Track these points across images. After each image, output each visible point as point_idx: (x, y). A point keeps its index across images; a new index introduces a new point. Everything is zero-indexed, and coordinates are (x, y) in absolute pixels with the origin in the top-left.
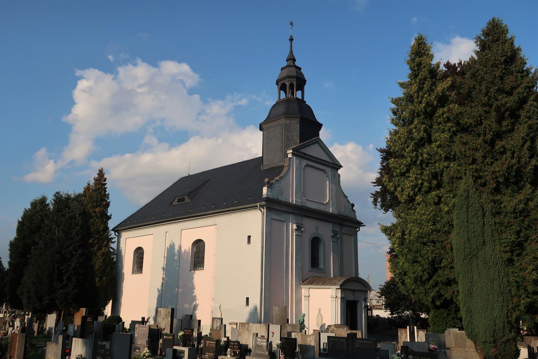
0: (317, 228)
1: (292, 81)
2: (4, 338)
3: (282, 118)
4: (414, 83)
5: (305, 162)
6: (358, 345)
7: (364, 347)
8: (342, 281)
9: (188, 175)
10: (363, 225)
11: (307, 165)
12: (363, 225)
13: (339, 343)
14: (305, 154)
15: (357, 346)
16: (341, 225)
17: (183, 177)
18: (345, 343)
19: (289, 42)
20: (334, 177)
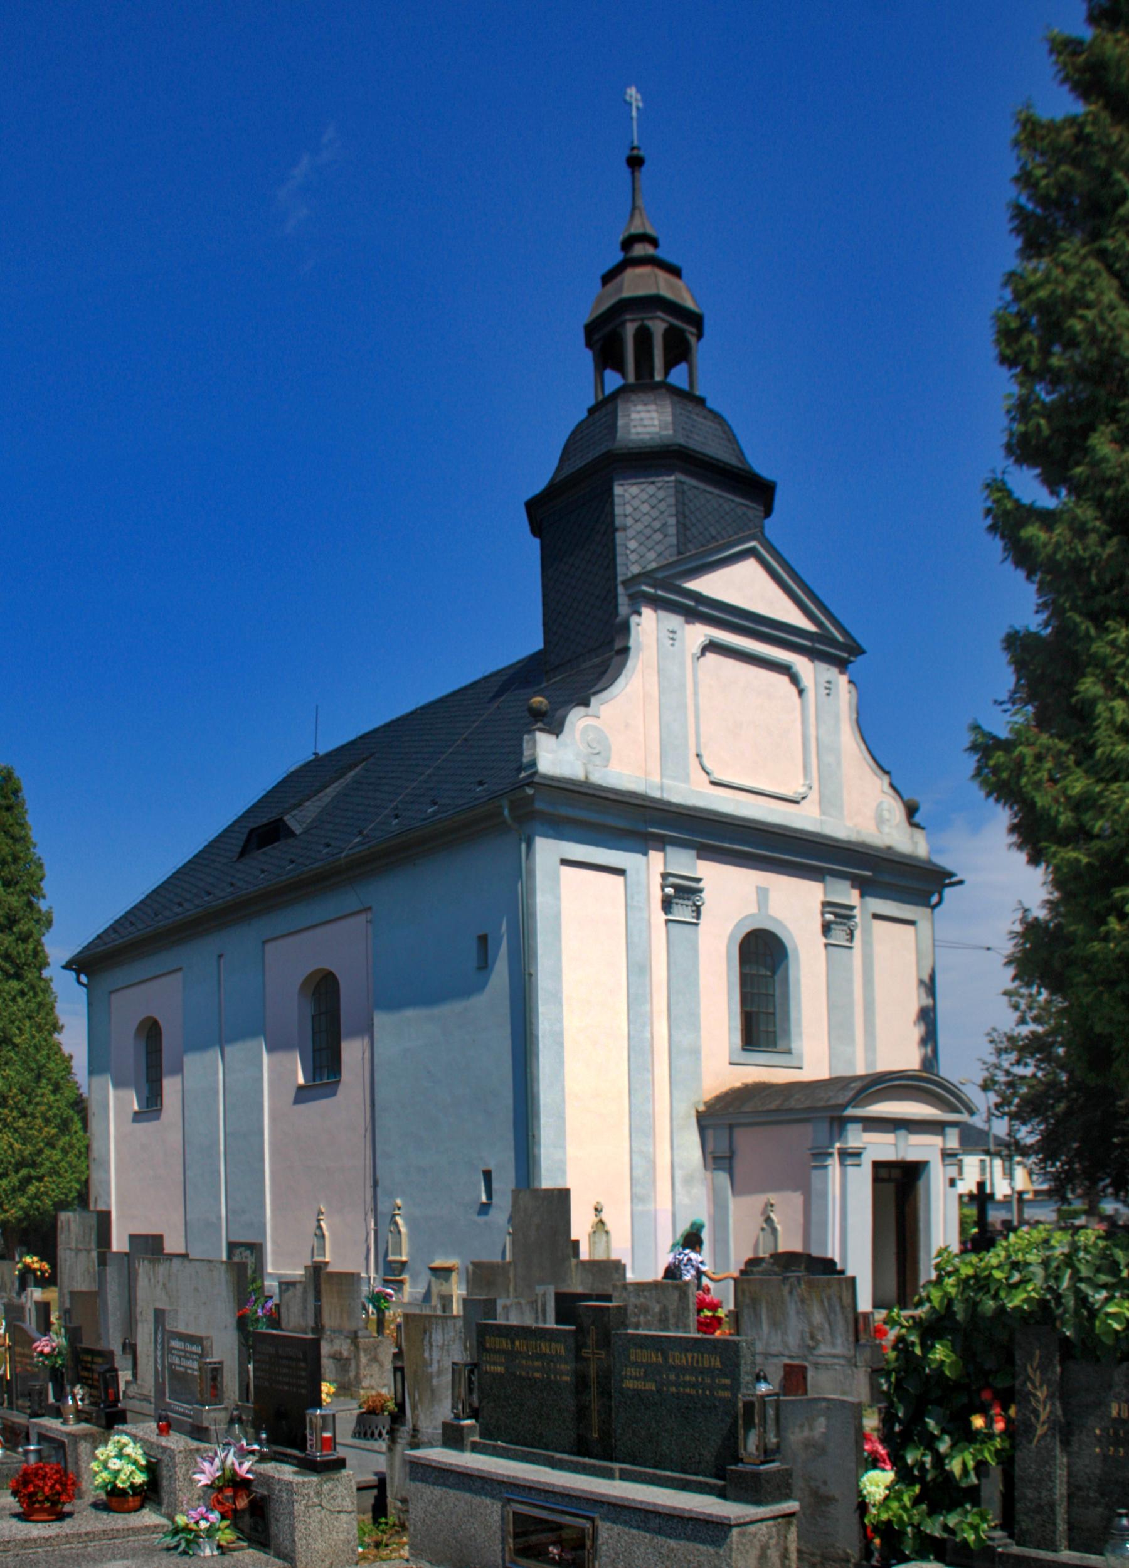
0: (763, 894)
1: (642, 320)
2: (258, 1374)
3: (988, 1170)
4: (1116, 1433)
5: (700, 633)
6: (636, 1378)
7: (673, 1389)
8: (852, 1089)
9: (313, 757)
10: (954, 879)
11: (712, 647)
12: (954, 879)
13: (537, 1364)
14: (698, 597)
15: (629, 1384)
16: (866, 888)
17: (719, 1098)
18: (563, 1367)
19: (626, 171)
20: (828, 695)
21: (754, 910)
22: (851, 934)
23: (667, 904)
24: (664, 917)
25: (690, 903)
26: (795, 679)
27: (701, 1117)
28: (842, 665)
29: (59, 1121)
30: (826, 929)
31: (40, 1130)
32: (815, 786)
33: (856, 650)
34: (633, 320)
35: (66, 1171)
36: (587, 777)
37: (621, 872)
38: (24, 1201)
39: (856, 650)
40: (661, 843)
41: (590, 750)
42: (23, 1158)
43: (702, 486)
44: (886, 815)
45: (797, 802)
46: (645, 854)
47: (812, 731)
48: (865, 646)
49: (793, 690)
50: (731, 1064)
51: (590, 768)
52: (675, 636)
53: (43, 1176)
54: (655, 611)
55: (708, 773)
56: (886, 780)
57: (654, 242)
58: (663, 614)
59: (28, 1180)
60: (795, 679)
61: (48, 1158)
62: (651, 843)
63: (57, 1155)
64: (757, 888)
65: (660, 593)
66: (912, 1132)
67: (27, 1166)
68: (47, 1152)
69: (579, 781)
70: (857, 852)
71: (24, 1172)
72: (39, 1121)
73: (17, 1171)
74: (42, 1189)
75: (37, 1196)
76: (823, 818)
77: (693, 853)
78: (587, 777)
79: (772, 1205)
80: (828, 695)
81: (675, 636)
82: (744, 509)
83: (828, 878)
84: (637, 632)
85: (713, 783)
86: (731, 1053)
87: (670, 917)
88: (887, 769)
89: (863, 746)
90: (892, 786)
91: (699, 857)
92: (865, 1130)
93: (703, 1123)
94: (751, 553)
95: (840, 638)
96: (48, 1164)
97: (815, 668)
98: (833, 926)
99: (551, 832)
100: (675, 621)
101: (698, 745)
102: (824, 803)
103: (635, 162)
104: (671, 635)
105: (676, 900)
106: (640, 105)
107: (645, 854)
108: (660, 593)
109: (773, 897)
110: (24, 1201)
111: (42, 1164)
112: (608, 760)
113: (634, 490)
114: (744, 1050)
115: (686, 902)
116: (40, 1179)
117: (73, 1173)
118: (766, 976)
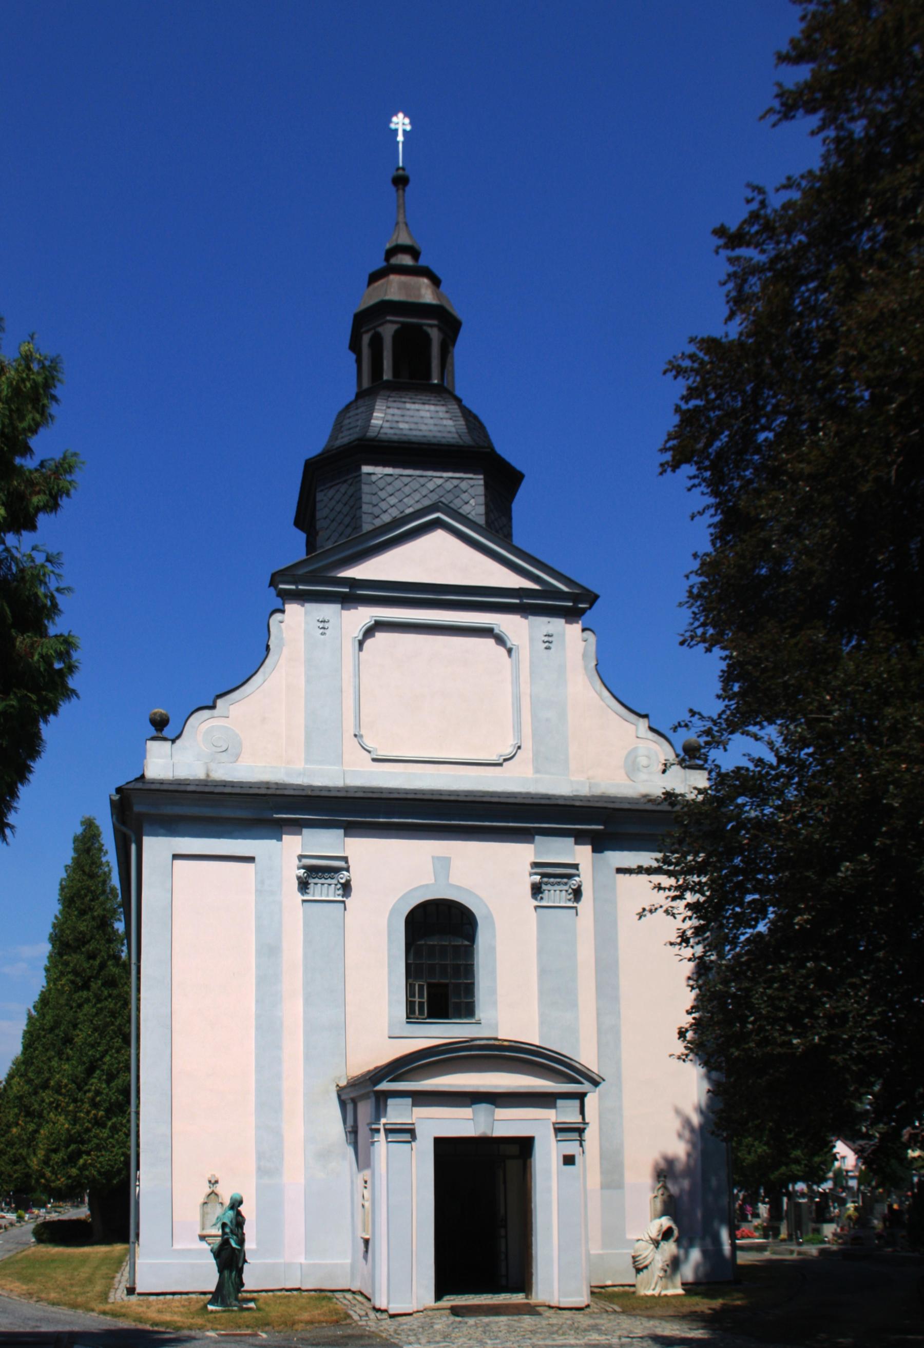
5: (366, 615)
21: (429, 879)
22: (577, 894)
23: (303, 885)
24: (300, 897)
25: (334, 881)
26: (500, 640)
27: (340, 1091)
28: (571, 615)
29: (108, 1105)
30: (537, 890)
31: (88, 1113)
32: (527, 745)
33: (592, 598)
34: (367, 332)
35: (113, 1146)
36: (208, 775)
37: (251, 859)
38: (74, 1171)
39: (592, 598)
40: (297, 826)
41: (215, 749)
42: (71, 1136)
43: (418, 473)
44: (643, 761)
45: (500, 765)
46: (280, 839)
47: (525, 688)
48: (596, 590)
49: (502, 651)
50: (390, 1037)
51: (213, 766)
52: (326, 625)
53: (91, 1150)
54: (303, 606)
55: (369, 752)
56: (643, 724)
57: (414, 253)
58: (309, 606)
59: (79, 1154)
60: (500, 640)
61: (96, 1136)
62: (285, 829)
63: (105, 1133)
64: (433, 857)
65: (300, 587)
66: (498, 1105)
67: (76, 1142)
68: (96, 1131)
69: (200, 780)
70: (573, 806)
71: (73, 1147)
72: (86, 1106)
73: (67, 1146)
74: (90, 1161)
75: (85, 1167)
76: (538, 776)
77: (341, 832)
78: (208, 775)
79: (210, 1182)
80: (547, 648)
81: (326, 625)
82: (456, 482)
83: (537, 838)
84: (280, 630)
85: (374, 760)
86: (391, 1026)
87: (306, 898)
88: (643, 713)
89: (606, 693)
90: (651, 729)
91: (346, 835)
92: (414, 1104)
93: (343, 1097)
94: (437, 524)
95: (565, 589)
96: (96, 1141)
97: (531, 627)
98: (544, 887)
99: (162, 831)
100: (329, 610)
101: (358, 724)
102: (540, 762)
103: (401, 181)
104: (321, 625)
105: (311, 881)
106: (408, 128)
107: (280, 839)
108: (300, 587)
109: (456, 865)
110: (74, 1171)
111: (89, 1141)
112: (237, 756)
113: (331, 493)
114: (408, 1022)
115: (329, 881)
116: (88, 1153)
117: (121, 1148)
118: (466, 946)
